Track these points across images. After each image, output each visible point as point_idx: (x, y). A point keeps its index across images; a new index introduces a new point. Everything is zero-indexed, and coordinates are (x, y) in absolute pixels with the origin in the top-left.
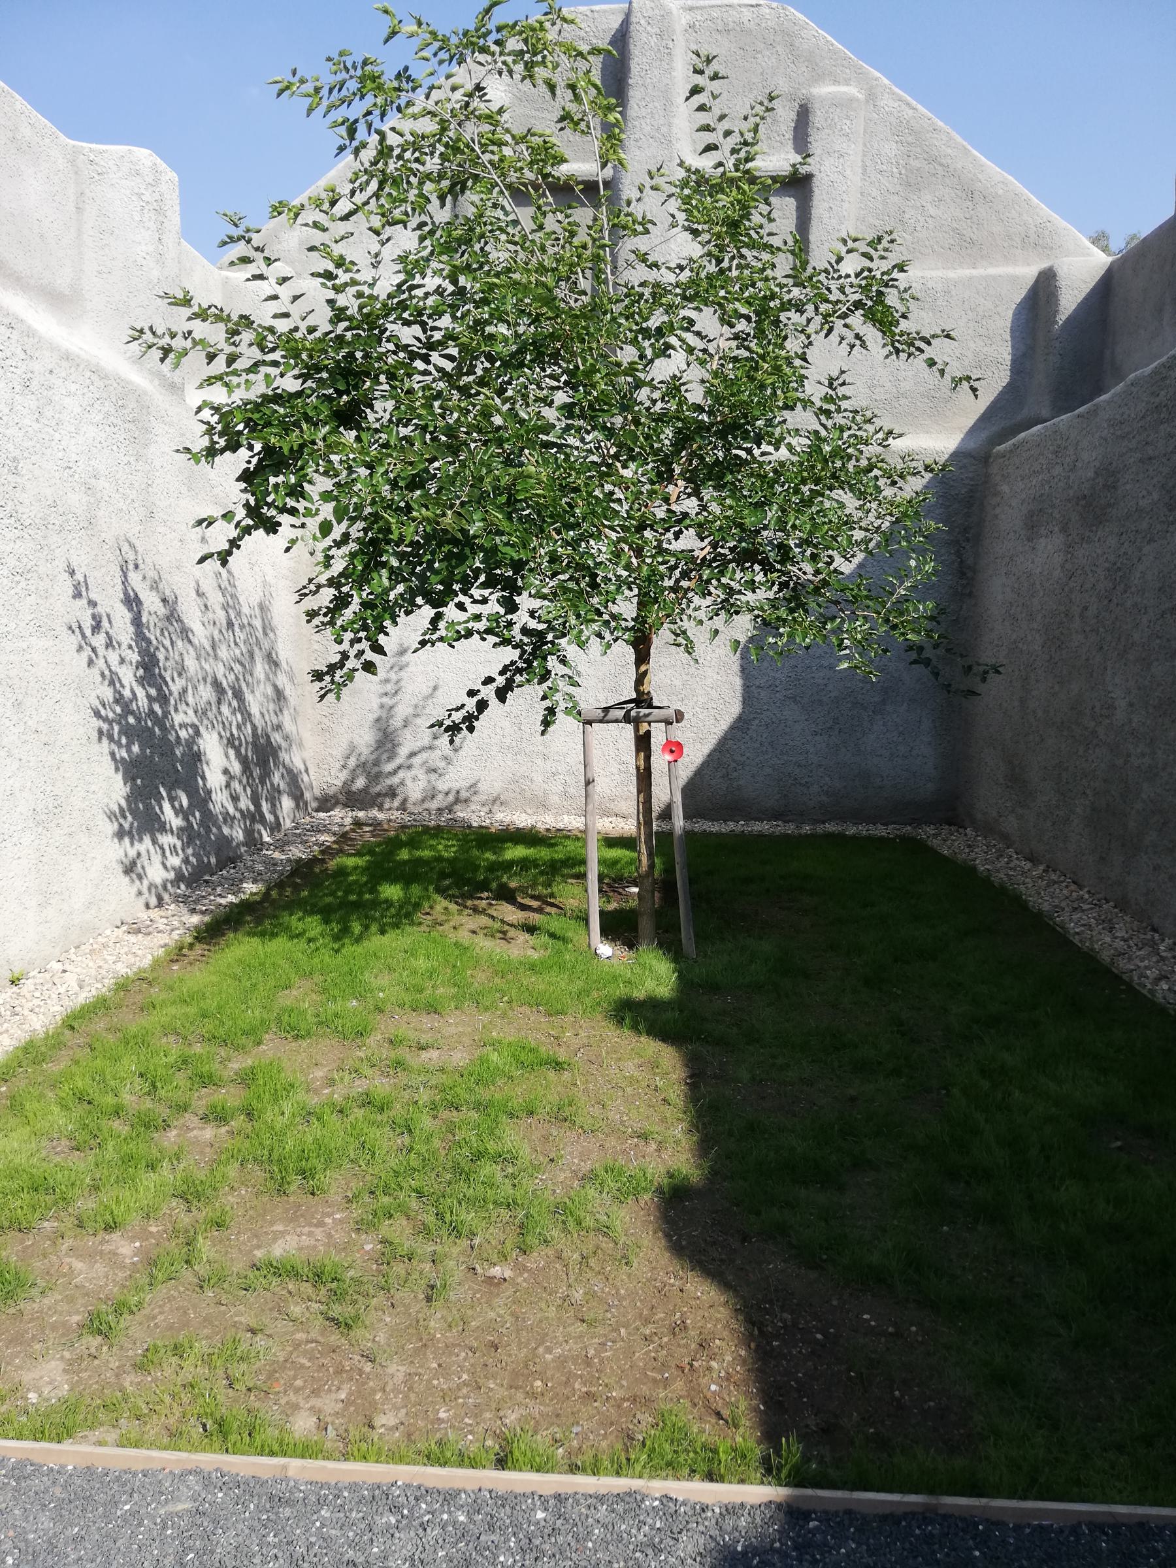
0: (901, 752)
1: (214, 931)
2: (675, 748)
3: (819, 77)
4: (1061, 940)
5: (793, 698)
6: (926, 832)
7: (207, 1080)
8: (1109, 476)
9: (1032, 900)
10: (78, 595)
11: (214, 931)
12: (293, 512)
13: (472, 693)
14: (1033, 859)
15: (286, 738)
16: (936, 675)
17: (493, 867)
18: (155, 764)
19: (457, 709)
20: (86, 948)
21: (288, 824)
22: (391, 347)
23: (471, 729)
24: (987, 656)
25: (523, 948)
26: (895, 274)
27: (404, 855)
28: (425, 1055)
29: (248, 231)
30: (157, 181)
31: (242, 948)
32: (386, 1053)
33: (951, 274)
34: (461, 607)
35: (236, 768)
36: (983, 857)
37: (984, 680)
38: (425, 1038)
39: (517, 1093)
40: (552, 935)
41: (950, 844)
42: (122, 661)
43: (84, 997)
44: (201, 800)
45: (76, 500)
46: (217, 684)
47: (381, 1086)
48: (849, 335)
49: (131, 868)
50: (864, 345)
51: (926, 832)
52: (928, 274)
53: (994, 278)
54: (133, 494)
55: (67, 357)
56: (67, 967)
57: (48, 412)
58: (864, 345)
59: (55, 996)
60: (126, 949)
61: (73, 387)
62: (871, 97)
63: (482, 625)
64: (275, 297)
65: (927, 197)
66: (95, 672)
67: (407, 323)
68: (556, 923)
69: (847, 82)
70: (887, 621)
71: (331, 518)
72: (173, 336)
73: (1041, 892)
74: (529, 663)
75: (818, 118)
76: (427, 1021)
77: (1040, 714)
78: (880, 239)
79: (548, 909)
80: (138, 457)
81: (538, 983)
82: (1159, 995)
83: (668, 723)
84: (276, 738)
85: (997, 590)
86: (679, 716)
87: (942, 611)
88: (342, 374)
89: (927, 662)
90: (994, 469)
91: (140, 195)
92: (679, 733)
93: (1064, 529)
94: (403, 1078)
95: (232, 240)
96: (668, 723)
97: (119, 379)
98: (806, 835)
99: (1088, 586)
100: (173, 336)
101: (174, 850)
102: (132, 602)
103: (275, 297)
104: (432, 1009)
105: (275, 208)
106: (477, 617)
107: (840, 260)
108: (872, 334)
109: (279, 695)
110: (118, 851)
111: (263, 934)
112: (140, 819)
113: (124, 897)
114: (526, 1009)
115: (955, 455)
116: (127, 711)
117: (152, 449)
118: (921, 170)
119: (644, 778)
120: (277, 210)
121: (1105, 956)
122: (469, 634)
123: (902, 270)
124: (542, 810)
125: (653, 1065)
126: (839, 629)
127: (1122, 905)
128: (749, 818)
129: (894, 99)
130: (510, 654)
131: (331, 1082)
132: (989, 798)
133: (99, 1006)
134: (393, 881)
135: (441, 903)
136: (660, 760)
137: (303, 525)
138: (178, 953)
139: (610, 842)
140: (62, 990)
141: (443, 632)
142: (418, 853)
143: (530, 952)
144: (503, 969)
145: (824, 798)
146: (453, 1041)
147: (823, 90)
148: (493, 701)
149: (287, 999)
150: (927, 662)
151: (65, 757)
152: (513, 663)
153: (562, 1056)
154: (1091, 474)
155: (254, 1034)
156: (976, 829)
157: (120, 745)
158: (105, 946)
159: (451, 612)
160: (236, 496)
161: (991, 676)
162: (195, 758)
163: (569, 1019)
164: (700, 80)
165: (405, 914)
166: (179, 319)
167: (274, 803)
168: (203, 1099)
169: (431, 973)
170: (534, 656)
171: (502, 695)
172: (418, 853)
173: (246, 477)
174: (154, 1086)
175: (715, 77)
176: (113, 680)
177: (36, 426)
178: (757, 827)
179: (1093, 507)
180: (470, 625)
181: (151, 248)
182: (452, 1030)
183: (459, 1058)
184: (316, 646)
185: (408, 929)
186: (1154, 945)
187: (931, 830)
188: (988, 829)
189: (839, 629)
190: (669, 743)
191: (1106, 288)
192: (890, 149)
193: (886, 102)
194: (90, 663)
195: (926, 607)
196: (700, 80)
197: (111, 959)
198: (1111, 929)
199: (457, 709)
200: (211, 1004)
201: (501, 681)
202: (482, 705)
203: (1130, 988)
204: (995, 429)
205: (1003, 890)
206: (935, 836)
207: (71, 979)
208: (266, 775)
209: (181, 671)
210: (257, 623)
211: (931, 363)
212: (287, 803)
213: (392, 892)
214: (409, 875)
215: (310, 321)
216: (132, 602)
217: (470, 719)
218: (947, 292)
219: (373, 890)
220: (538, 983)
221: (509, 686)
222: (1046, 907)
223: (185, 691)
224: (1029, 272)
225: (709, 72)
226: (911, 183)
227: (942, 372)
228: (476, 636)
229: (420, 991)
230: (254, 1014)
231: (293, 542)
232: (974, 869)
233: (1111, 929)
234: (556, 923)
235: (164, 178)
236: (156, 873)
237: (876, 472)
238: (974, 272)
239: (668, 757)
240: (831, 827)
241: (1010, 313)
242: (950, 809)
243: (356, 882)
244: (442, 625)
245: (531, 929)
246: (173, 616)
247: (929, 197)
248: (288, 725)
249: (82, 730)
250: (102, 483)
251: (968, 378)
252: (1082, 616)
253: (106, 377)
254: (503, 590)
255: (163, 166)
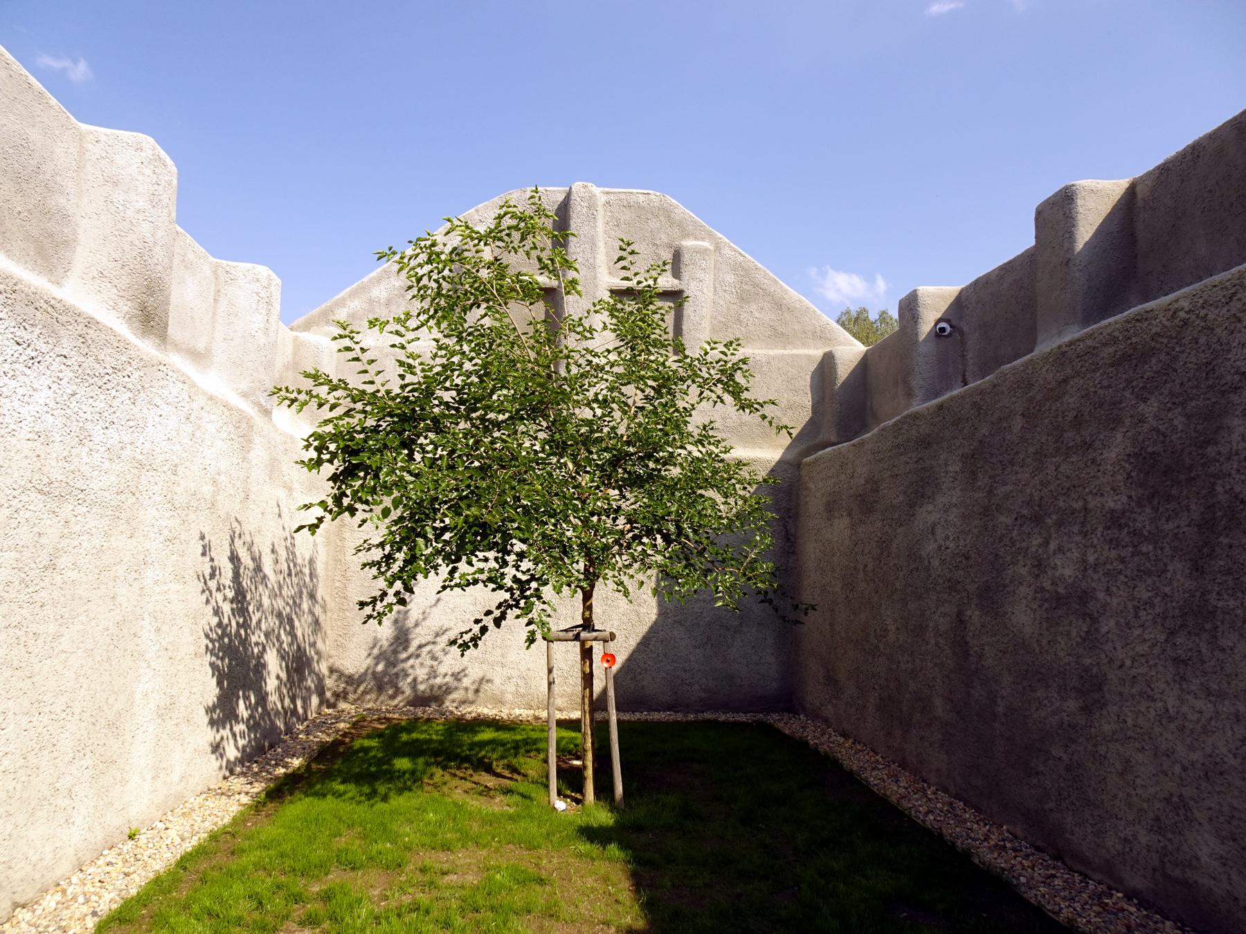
0: (753, 660)
1: (279, 792)
2: (609, 658)
3: (686, 235)
4: (864, 789)
5: (680, 622)
6: (773, 718)
7: (297, 898)
8: (874, 483)
9: (846, 763)
10: (204, 554)
11: (279, 792)
12: (367, 502)
13: (477, 621)
14: (845, 735)
15: (318, 653)
16: (776, 610)
17: (473, 745)
18: (236, 669)
19: (466, 633)
20: (178, 811)
21: (312, 715)
22: (436, 402)
23: (476, 646)
24: (807, 596)
25: (499, 805)
26: (741, 365)
27: (404, 737)
28: (447, 878)
29: (352, 332)
30: (269, 285)
31: (298, 807)
32: (419, 877)
33: (771, 352)
34: (470, 563)
35: (284, 676)
36: (812, 735)
37: (806, 614)
38: (446, 867)
39: (518, 899)
40: (523, 796)
41: (789, 726)
42: (225, 599)
43: (188, 847)
44: (262, 698)
45: (207, 490)
46: (279, 615)
47: (423, 898)
48: (714, 396)
49: (216, 748)
50: (722, 401)
51: (773, 718)
52: (756, 351)
53: (797, 356)
54: (238, 484)
55: (211, 398)
56: (168, 825)
57: (198, 434)
58: (722, 401)
59: (164, 847)
60: (208, 812)
61: (212, 417)
62: (718, 248)
63: (484, 577)
64: (366, 372)
65: (754, 307)
66: (210, 608)
67: (447, 389)
68: (522, 786)
69: (703, 239)
70: (744, 575)
71: (390, 505)
72: (299, 392)
73: (852, 758)
74: (518, 602)
75: (686, 258)
76: (443, 856)
77: (843, 634)
78: (731, 343)
79: (516, 776)
80: (244, 459)
81: (518, 828)
82: (928, 823)
83: (605, 641)
84: (310, 652)
85: (811, 551)
86: (613, 636)
87: (777, 569)
88: (407, 418)
89: (771, 601)
90: (804, 473)
91: (257, 294)
92: (612, 647)
93: (849, 514)
94: (435, 893)
95: (341, 337)
96: (605, 641)
97: (239, 410)
98: (692, 722)
99: (866, 551)
100: (299, 392)
101: (243, 735)
102: (234, 558)
103: (366, 372)
104: (446, 847)
105: (371, 322)
106: (481, 571)
107: (706, 353)
108: (728, 398)
109: (317, 622)
110: (210, 734)
111: (316, 794)
112: (222, 713)
113: (211, 767)
114: (512, 846)
115: (779, 462)
116: (224, 634)
117: (252, 453)
118: (749, 290)
119: (588, 679)
120: (372, 324)
121: (894, 799)
122: (476, 582)
123: (745, 363)
124: (499, 705)
125: (605, 880)
126: (716, 579)
127: (903, 765)
128: (650, 710)
129: (731, 250)
130: (504, 595)
131: (386, 898)
132: (814, 693)
133: (200, 853)
134: (403, 756)
135: (438, 772)
136: (599, 666)
137: (371, 510)
138: (257, 807)
139: (561, 724)
140: (168, 842)
141: (458, 581)
142: (414, 735)
143: (506, 808)
144: (489, 820)
145: (703, 695)
146: (464, 869)
147: (688, 243)
148: (491, 625)
149: (341, 843)
150: (771, 601)
151: (180, 667)
152: (506, 601)
153: (544, 875)
154: (863, 482)
155: (323, 867)
156: (806, 716)
157: (218, 658)
158: (193, 810)
159: (463, 567)
160: (326, 490)
161: (810, 612)
162: (261, 666)
163: (542, 852)
164: (624, 254)
165: (411, 782)
166: (308, 384)
167: (306, 701)
168: (298, 912)
169: (440, 824)
170: (522, 596)
171: (497, 622)
172: (414, 735)
173: (334, 478)
174: (261, 903)
175: (633, 253)
176: (217, 612)
177: (190, 443)
178: (656, 716)
179: (865, 502)
180: (476, 576)
181: (262, 326)
182: (462, 862)
183: (472, 879)
184: (337, 584)
185: (419, 793)
186: (924, 791)
187: (776, 716)
188: (815, 715)
189: (716, 579)
190: (606, 654)
191: (864, 365)
192: (730, 278)
193: (726, 251)
194: (208, 602)
195: (767, 566)
196: (624, 254)
197: (199, 819)
198: (897, 781)
199: (466, 633)
200: (287, 847)
201: (497, 613)
202: (484, 630)
203: (910, 820)
204: (804, 447)
205: (827, 757)
206: (780, 720)
207: (173, 833)
208: (302, 679)
209: (259, 606)
210: (307, 571)
211: (764, 417)
212: (315, 700)
213: (402, 764)
214: (414, 750)
215: (387, 387)
216: (234, 558)
217: (475, 640)
218: (769, 363)
219: (389, 762)
220: (518, 828)
221: (503, 616)
222: (855, 768)
223: (260, 621)
224: (818, 353)
225: (629, 250)
226: (744, 299)
227: (771, 423)
228: (480, 585)
229: (436, 835)
230: (319, 854)
231: (364, 521)
232: (807, 743)
233: (897, 781)
234: (522, 786)
235: (274, 283)
236: (232, 753)
237: (733, 481)
238: (785, 352)
239: (606, 665)
240: (708, 715)
241: (808, 378)
242: (788, 701)
243: (375, 757)
244: (457, 575)
245: (508, 791)
246: (258, 569)
247: (755, 307)
248: (320, 645)
249: (193, 648)
250: (222, 478)
251: (786, 427)
252: (864, 571)
253: (231, 409)
254: (498, 552)
255: (273, 276)
